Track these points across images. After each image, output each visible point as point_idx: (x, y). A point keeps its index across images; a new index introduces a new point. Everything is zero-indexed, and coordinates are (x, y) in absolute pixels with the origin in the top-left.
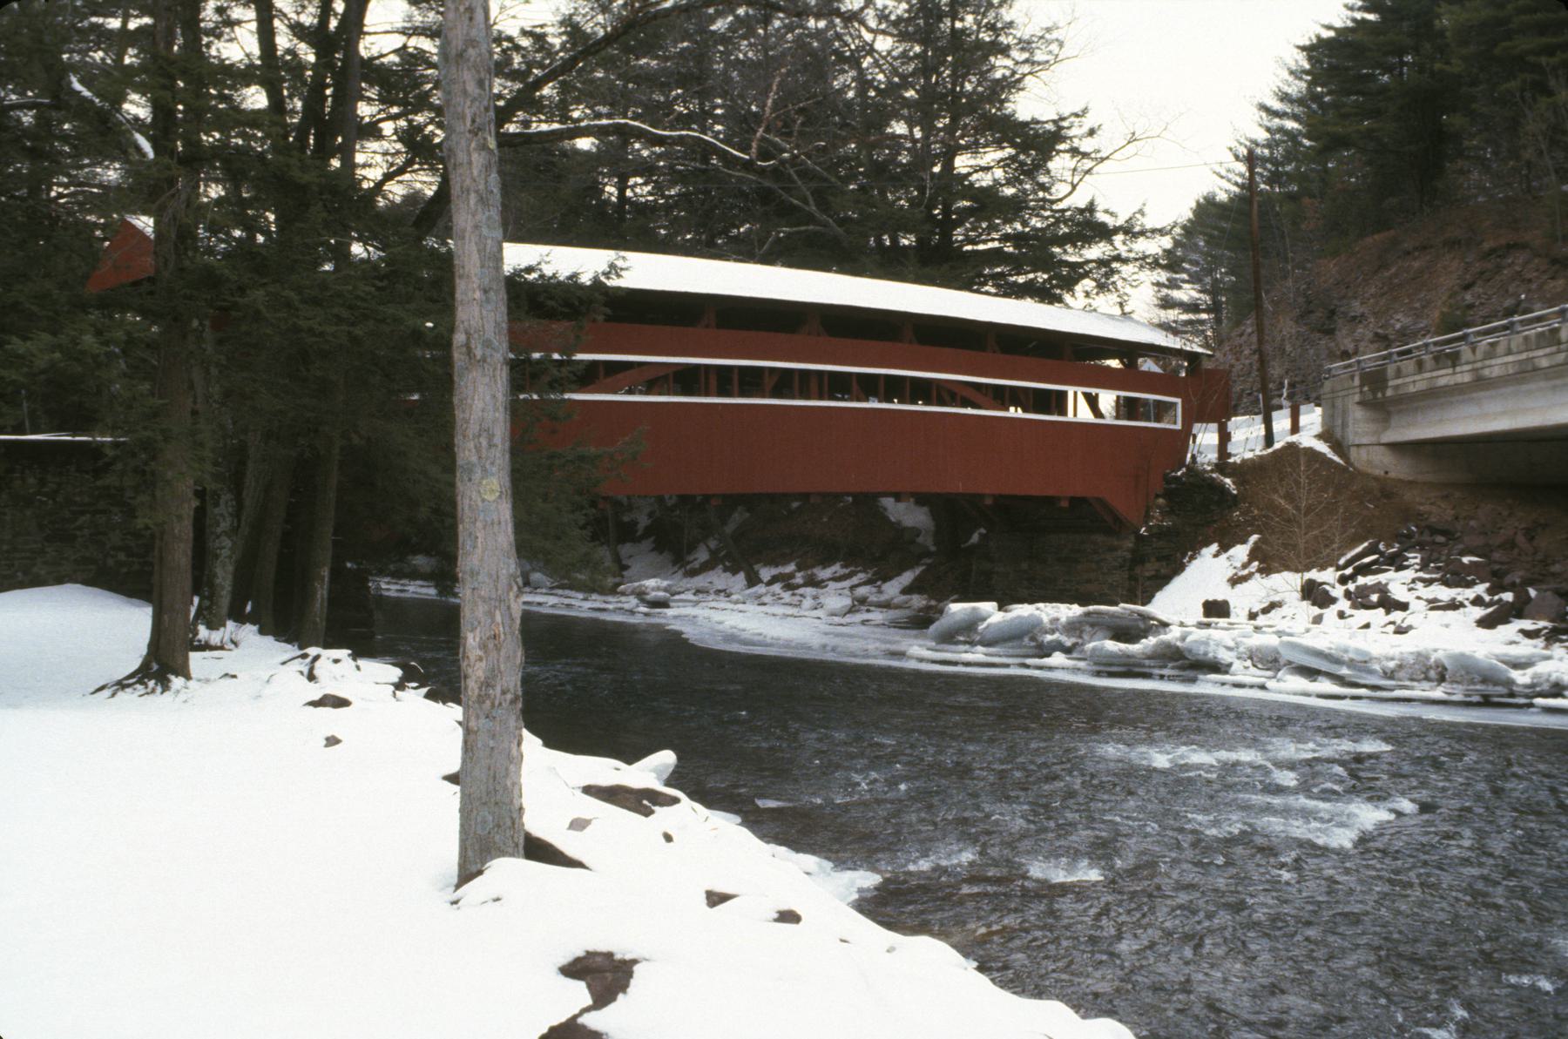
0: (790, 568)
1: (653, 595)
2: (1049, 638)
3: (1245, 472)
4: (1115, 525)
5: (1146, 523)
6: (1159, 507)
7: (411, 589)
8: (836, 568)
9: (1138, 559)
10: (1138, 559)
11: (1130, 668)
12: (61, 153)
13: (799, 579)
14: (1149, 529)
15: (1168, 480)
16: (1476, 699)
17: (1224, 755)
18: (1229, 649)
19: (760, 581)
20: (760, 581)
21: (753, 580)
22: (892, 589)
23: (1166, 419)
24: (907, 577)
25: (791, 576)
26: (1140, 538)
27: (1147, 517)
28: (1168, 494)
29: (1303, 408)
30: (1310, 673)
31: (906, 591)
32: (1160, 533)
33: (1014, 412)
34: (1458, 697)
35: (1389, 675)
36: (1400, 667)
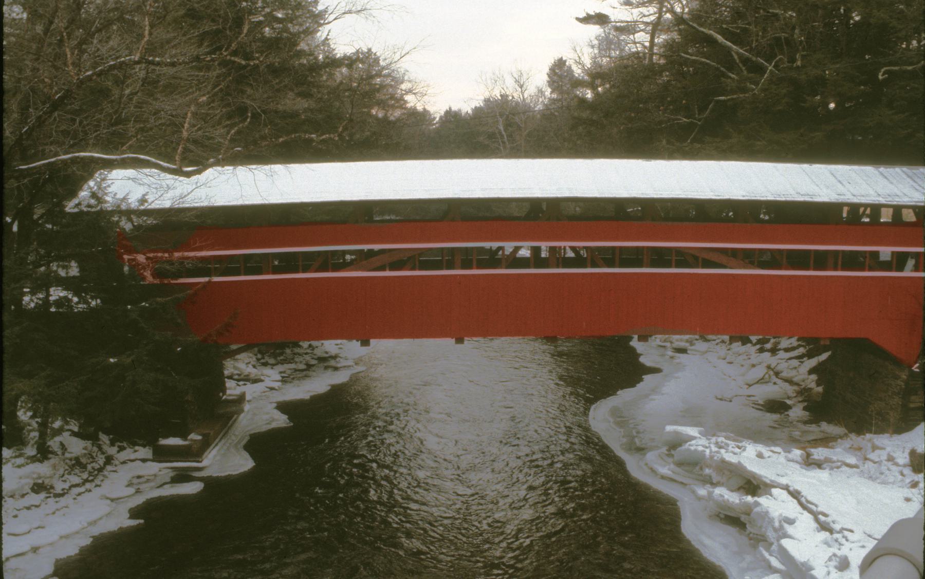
2: (707, 471)
20: (750, 342)
24: (813, 362)
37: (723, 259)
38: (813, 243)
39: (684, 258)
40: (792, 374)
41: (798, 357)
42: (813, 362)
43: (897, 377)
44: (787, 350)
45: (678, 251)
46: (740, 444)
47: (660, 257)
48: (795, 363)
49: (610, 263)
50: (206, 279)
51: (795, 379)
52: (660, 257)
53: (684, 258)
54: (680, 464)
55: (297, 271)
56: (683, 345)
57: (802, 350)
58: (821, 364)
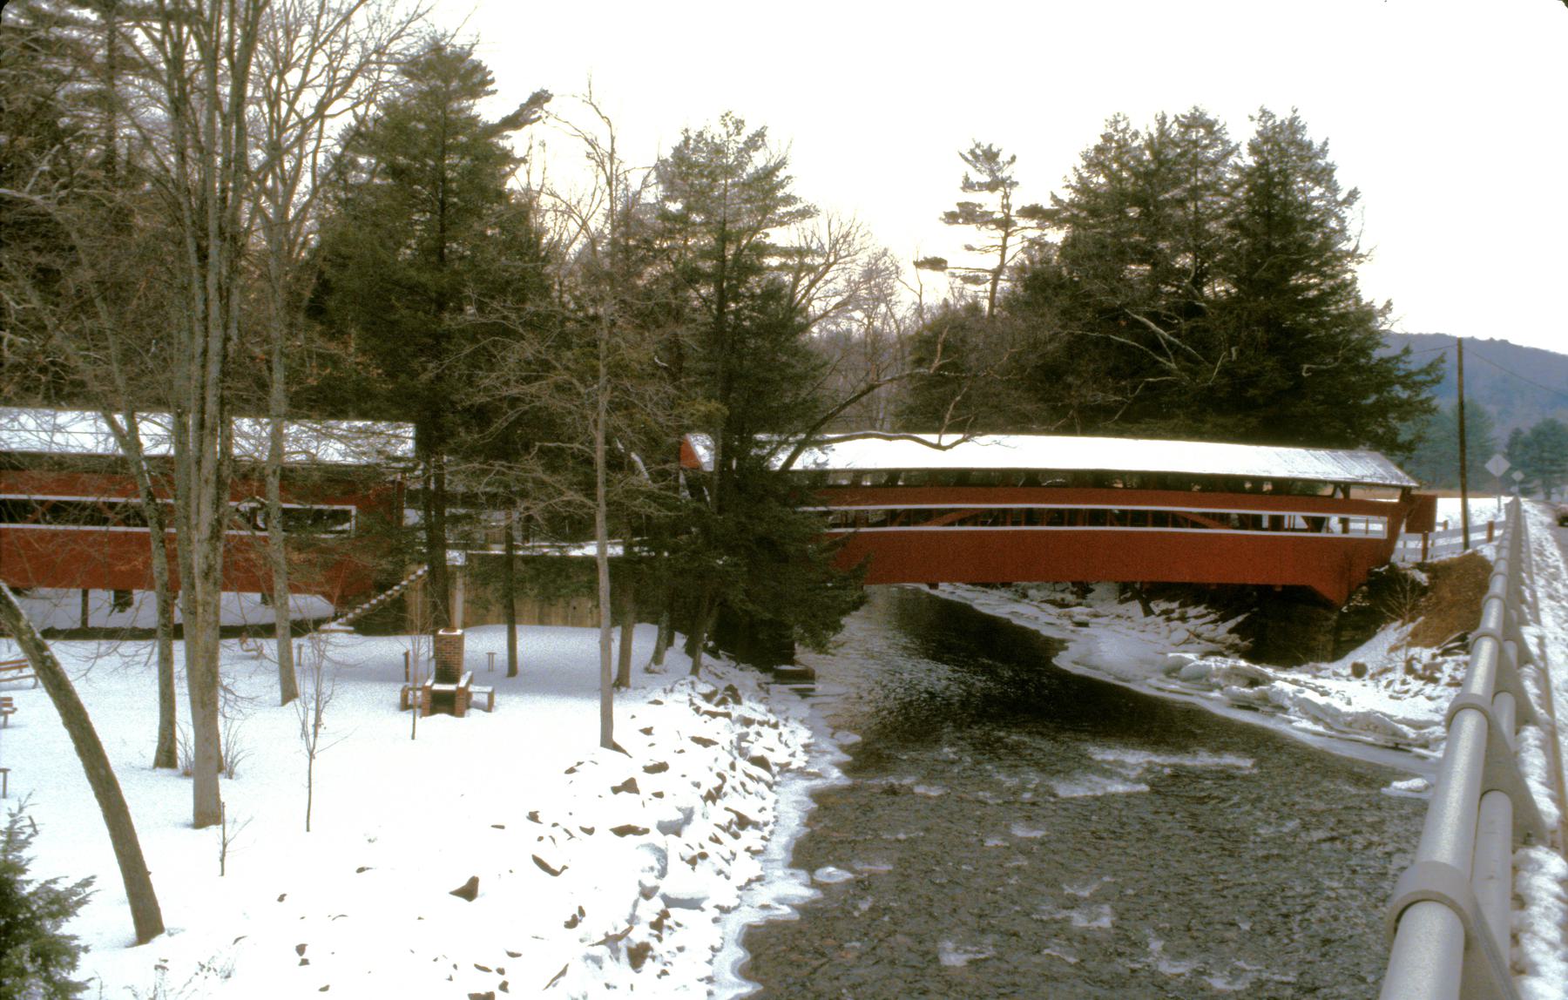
0: (1175, 605)
1: (1078, 618)
2: (1214, 680)
3: (1436, 571)
4: (1329, 605)
5: (1347, 602)
6: (1362, 592)
7: (959, 592)
8: (1201, 609)
9: (1338, 629)
10: (1338, 629)
11: (1248, 706)
12: (416, 131)
13: (1175, 615)
14: (1349, 607)
15: (1370, 573)
16: (1390, 744)
17: (1175, 760)
18: (1290, 699)
19: (1153, 613)
20: (1153, 613)
21: (1148, 612)
22: (1224, 628)
23: (1324, 530)
24: (1232, 623)
25: (1173, 611)
26: (1342, 614)
27: (1349, 599)
28: (1370, 584)
29: (518, 627)
30: (1316, 720)
31: (1231, 631)
32: (1358, 611)
33: (1234, 512)
34: (1381, 742)
35: (1350, 725)
36: (1356, 721)
37: (1207, 522)
38: (1211, 507)
39: (1177, 520)
40: (1212, 635)
41: (1212, 622)
42: (1232, 623)
43: (1327, 619)
44: (1196, 617)
45: (1174, 514)
46: (765, 913)
47: (1160, 519)
48: (1211, 626)
49: (962, 522)
50: (851, 530)
51: (1218, 638)
52: (1160, 519)
53: (1177, 520)
54: (1185, 680)
55: (1104, 524)
56: (1084, 618)
57: (1213, 617)
58: (1239, 624)
